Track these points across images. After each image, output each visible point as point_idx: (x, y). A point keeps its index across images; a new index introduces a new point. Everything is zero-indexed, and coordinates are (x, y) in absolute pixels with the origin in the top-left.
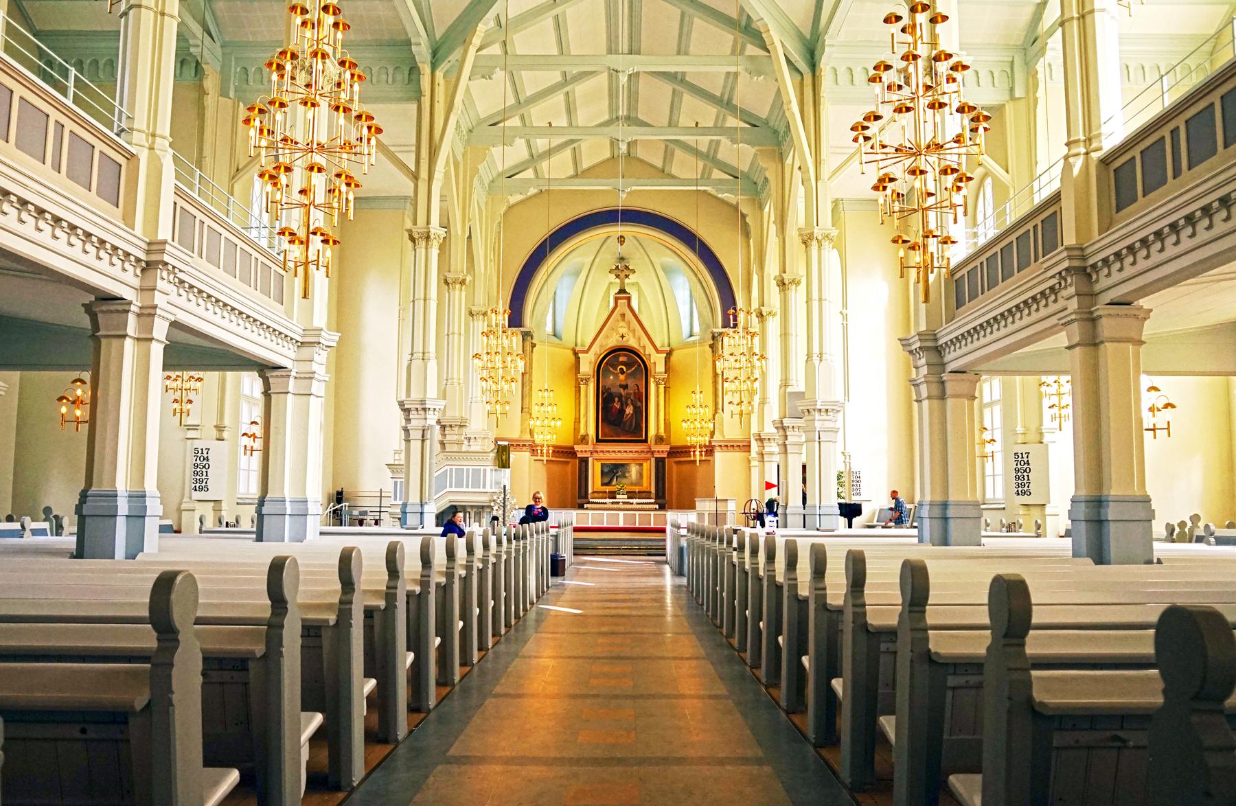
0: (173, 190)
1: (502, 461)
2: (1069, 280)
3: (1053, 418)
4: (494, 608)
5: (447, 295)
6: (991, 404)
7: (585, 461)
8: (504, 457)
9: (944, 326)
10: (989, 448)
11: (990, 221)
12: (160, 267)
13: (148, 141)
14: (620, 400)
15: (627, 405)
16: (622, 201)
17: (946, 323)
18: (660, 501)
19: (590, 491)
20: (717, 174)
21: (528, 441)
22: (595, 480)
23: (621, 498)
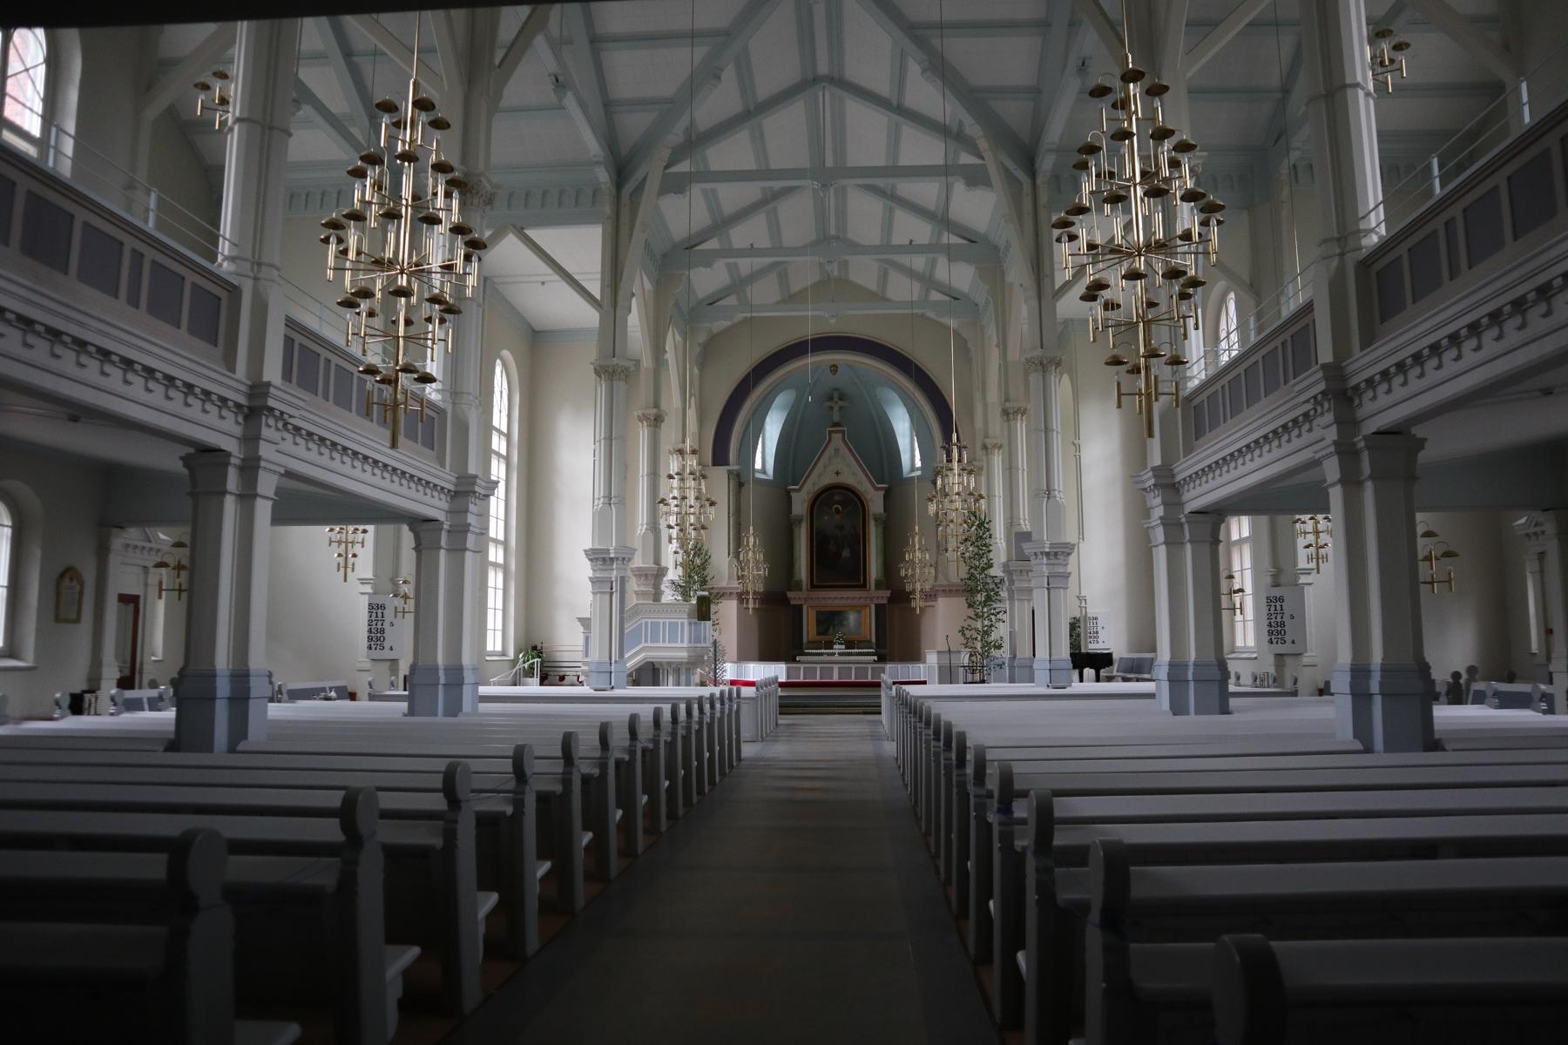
0: (284, 322)
2: (1326, 405)
3: (1309, 559)
4: (709, 759)
6: (1241, 541)
7: (800, 608)
8: (704, 609)
9: (1182, 460)
10: (1237, 598)
11: (1234, 337)
12: (265, 412)
13: (252, 270)
16: (809, 331)
17: (1362, 349)
19: (805, 640)
20: (935, 296)
22: (809, 628)
23: (838, 648)
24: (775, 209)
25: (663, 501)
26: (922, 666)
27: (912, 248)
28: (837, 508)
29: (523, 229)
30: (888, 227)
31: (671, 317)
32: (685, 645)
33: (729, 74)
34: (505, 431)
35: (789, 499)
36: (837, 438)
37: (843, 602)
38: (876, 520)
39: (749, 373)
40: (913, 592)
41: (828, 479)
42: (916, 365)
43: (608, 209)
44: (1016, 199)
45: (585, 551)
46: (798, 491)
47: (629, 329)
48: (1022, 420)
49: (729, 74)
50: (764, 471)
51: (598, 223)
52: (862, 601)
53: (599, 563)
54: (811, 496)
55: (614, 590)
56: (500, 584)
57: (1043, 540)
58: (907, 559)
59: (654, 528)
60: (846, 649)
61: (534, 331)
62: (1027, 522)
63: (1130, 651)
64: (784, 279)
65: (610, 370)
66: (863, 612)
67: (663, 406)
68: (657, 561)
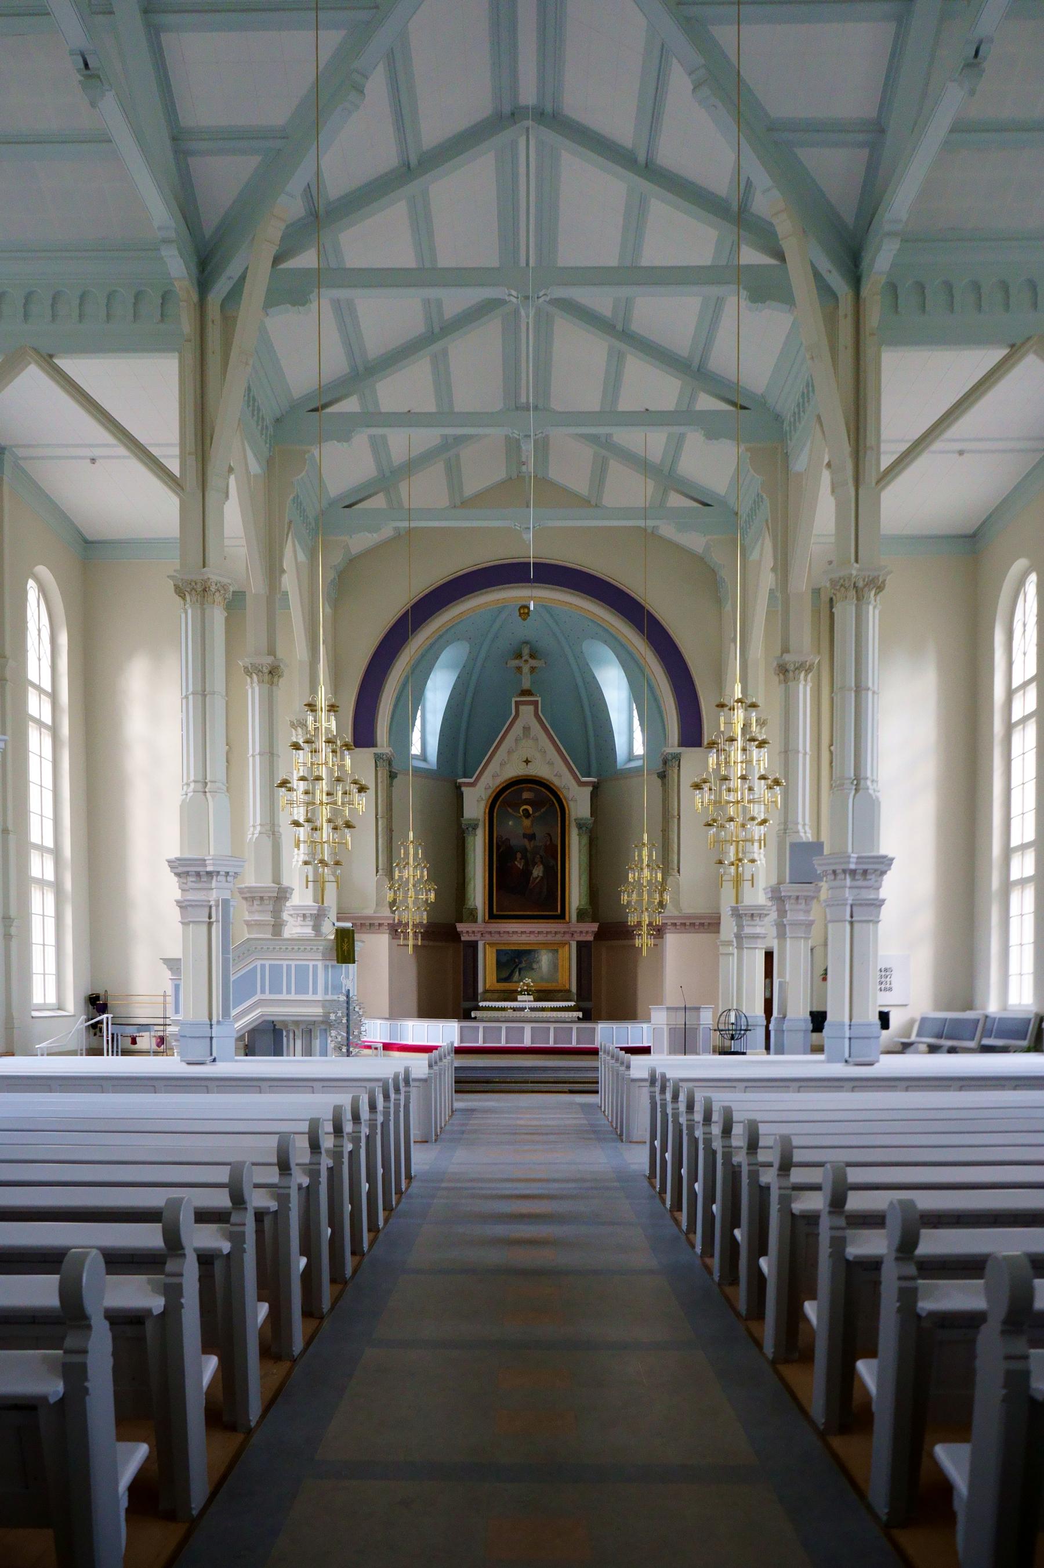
1: (343, 952)
4: (369, 1193)
5: (250, 691)
7: (473, 946)
8: (345, 947)
14: (524, 857)
15: (534, 864)
18: (585, 1004)
19: (480, 990)
20: (676, 500)
21: (387, 918)
24: (445, 352)
25: (284, 783)
26: (645, 1026)
27: (648, 418)
28: (526, 810)
29: (51, 356)
30: (613, 382)
31: (290, 522)
32: (319, 997)
33: (377, 84)
34: (49, 689)
35: (460, 796)
36: (527, 711)
37: (532, 938)
38: (580, 826)
39: (407, 612)
40: (639, 924)
41: (514, 770)
42: (650, 614)
43: (187, 324)
44: (831, 321)
45: (169, 861)
46: (472, 785)
47: (227, 542)
48: (806, 680)
49: (377, 84)
50: (423, 757)
51: (173, 350)
52: (559, 938)
53: (299, 918)
54: (490, 791)
55: (213, 919)
56: (50, 910)
57: (847, 852)
58: (631, 880)
59: (272, 831)
60: (535, 1000)
61: (87, 542)
62: (807, 828)
63: (938, 1007)
64: (453, 472)
65: (199, 588)
66: (560, 951)
67: (280, 654)
68: (277, 878)
